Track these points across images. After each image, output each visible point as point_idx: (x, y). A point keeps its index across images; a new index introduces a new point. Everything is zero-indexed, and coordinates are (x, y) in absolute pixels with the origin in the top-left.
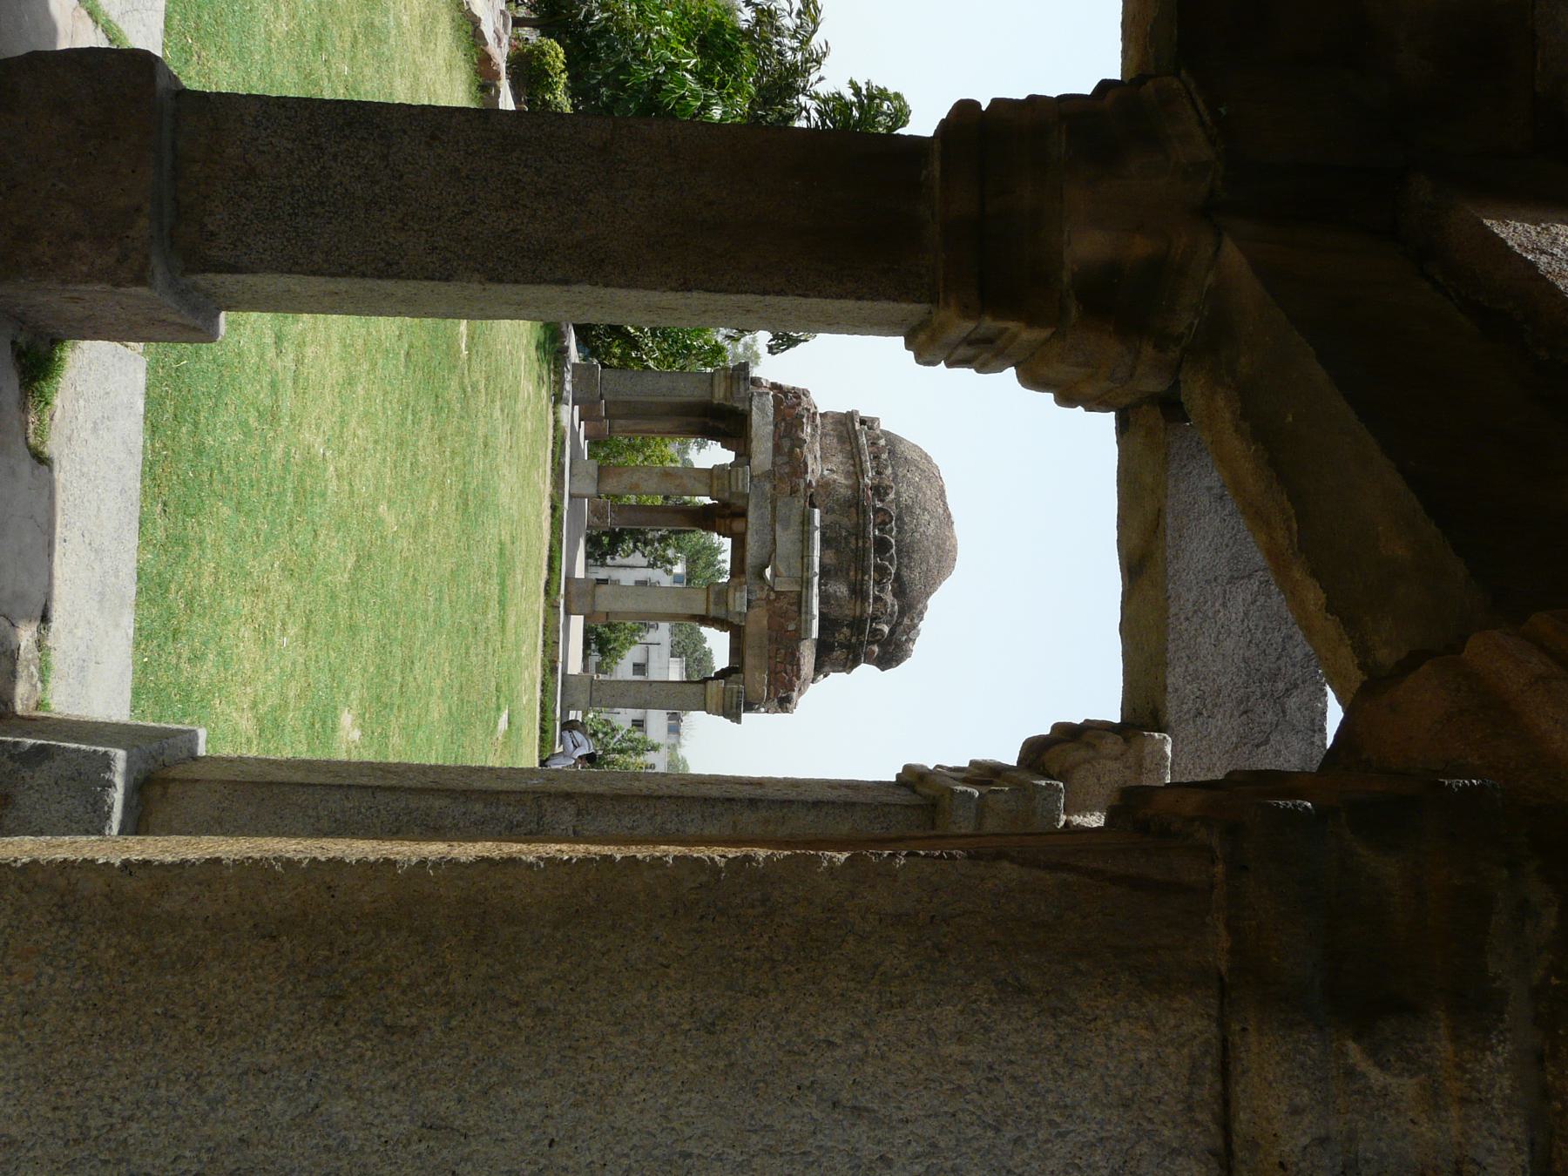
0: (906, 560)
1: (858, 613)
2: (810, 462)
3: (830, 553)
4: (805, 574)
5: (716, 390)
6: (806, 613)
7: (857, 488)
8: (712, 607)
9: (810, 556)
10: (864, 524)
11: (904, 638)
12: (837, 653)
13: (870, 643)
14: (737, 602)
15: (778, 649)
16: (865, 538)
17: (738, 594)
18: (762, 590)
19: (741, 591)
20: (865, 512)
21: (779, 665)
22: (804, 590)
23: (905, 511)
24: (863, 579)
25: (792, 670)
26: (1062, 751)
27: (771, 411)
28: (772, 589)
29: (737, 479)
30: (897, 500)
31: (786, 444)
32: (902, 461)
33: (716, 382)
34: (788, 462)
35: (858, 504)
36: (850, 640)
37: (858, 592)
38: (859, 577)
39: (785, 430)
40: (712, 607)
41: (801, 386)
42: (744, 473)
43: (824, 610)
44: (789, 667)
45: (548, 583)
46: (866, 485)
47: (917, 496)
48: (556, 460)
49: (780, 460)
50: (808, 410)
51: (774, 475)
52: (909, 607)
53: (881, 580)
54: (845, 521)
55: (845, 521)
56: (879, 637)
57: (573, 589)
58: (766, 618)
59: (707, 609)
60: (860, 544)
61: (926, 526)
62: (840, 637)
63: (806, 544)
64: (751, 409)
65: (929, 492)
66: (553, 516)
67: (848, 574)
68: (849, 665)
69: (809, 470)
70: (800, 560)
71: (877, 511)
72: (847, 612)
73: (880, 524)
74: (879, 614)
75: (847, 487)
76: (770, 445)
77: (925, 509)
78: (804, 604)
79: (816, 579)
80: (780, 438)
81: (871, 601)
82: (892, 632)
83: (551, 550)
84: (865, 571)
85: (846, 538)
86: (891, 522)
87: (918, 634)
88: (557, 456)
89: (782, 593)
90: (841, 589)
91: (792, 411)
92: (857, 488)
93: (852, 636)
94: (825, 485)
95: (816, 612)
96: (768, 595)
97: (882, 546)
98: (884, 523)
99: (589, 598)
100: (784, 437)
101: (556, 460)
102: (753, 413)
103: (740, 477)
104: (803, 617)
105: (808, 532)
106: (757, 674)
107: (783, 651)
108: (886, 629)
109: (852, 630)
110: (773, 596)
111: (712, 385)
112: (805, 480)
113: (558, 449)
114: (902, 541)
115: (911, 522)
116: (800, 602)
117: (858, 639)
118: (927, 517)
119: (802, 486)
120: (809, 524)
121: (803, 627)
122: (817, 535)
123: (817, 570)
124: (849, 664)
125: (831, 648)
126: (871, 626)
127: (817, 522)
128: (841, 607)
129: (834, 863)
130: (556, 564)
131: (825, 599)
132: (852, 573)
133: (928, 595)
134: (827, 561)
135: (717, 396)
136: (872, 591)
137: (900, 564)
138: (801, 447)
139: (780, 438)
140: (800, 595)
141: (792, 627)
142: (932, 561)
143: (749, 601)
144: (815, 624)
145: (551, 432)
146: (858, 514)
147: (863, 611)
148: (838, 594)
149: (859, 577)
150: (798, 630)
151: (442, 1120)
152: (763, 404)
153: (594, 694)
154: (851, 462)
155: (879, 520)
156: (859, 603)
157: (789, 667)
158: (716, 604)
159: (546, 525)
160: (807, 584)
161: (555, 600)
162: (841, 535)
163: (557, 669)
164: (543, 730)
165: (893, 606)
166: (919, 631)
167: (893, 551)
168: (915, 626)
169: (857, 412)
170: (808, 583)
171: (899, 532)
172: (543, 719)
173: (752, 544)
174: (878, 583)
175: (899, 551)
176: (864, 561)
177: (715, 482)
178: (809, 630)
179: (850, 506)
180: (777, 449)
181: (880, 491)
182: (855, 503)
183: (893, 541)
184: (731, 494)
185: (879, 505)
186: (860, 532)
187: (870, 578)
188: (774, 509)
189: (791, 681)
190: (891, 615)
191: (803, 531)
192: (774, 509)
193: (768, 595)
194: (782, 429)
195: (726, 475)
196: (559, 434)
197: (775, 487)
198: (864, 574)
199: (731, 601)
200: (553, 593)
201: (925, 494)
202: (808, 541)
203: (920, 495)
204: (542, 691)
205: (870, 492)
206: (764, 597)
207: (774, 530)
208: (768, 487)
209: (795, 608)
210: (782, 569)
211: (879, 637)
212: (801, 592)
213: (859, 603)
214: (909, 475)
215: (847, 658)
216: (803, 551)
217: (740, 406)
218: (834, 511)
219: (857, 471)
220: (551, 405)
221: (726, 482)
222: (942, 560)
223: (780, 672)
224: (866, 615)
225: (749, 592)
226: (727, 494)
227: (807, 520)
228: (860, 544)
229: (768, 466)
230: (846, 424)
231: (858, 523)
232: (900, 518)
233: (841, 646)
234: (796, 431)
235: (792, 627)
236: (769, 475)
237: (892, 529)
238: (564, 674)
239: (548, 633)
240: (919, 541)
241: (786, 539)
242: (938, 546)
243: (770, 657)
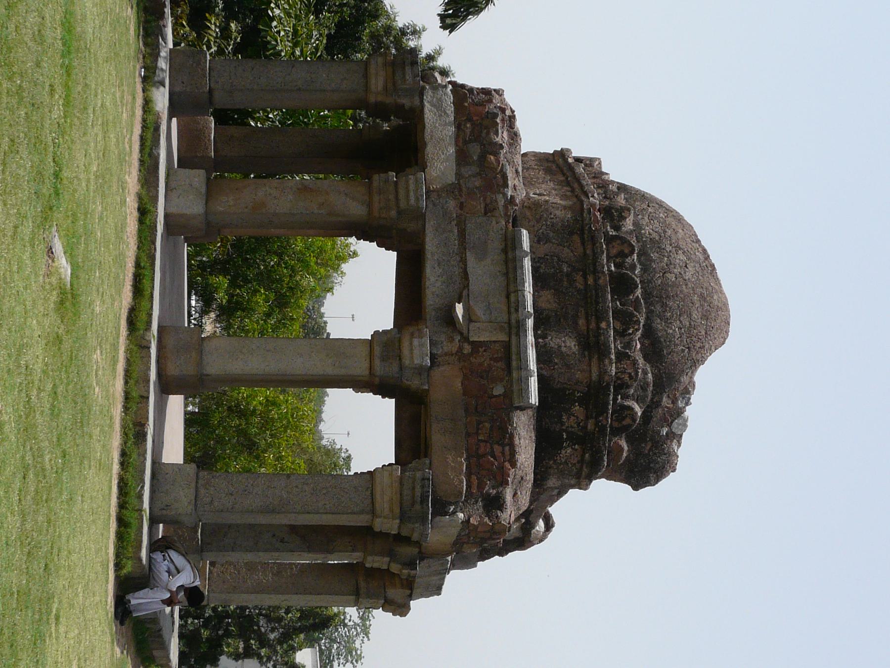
1: (595, 376)
2: (510, 174)
3: (547, 295)
4: (514, 316)
5: (373, 81)
6: (520, 368)
8: (377, 362)
9: (519, 291)
10: (594, 254)
11: (664, 431)
13: (616, 432)
14: (416, 352)
15: (479, 423)
16: (596, 272)
17: (416, 342)
18: (451, 340)
19: (421, 337)
20: (593, 239)
21: (482, 445)
22: (514, 338)
24: (599, 328)
25: (503, 453)
27: (451, 110)
28: (465, 339)
29: (408, 191)
31: (475, 150)
33: (372, 70)
34: (479, 174)
35: (582, 230)
36: (585, 427)
38: (593, 325)
39: (472, 132)
40: (377, 362)
41: (493, 86)
42: (417, 181)
43: (544, 372)
44: (497, 449)
45: (132, 311)
46: (593, 205)
47: (665, 232)
48: (147, 150)
49: (467, 171)
50: (503, 110)
51: (460, 190)
53: (625, 330)
54: (566, 253)
55: (566, 253)
56: (627, 421)
57: (170, 342)
58: (459, 380)
59: (371, 368)
60: (591, 281)
62: (569, 422)
63: (511, 276)
64: (422, 106)
66: (141, 221)
67: (576, 323)
70: (504, 299)
71: (610, 240)
72: (578, 375)
73: (616, 256)
74: (627, 378)
75: (565, 208)
76: (452, 150)
77: (678, 248)
78: (514, 357)
79: (530, 323)
80: (466, 142)
81: (613, 357)
82: (647, 416)
83: (138, 265)
84: (600, 317)
85: (568, 275)
86: (632, 252)
87: (685, 426)
88: (148, 143)
90: (569, 344)
91: (480, 108)
93: (587, 418)
94: (533, 207)
98: (622, 255)
99: (194, 354)
100: (470, 141)
101: (147, 150)
102: (426, 110)
103: (412, 187)
105: (514, 259)
106: (450, 459)
107: (487, 425)
108: (639, 410)
109: (587, 409)
110: (467, 349)
111: (366, 76)
112: (505, 195)
113: (149, 135)
114: (650, 282)
117: (596, 424)
119: (501, 202)
121: (515, 387)
122: (527, 263)
123: (530, 309)
124: (585, 470)
125: (558, 445)
126: (615, 399)
127: (526, 244)
128: (568, 366)
130: (146, 282)
132: (582, 322)
133: (695, 364)
134: (543, 305)
135: (373, 87)
136: (614, 345)
137: (650, 312)
138: (496, 154)
139: (466, 142)
140: (507, 346)
141: (498, 390)
142: (695, 315)
145: (139, 112)
146: (583, 244)
147: (603, 372)
148: (564, 349)
149: (593, 325)
150: (508, 395)
152: (440, 100)
153: (202, 491)
155: (614, 251)
156: (595, 361)
157: (497, 449)
158: (383, 359)
159: (132, 226)
160: (520, 327)
161: (143, 338)
162: (561, 271)
163: (145, 435)
164: (121, 522)
165: (645, 373)
166: (686, 420)
167: (639, 292)
168: (678, 413)
169: (568, 150)
170: (518, 327)
171: (645, 269)
172: (122, 506)
173: (432, 279)
174: (620, 334)
175: (647, 295)
176: (597, 303)
177: (376, 198)
178: (524, 391)
179: (571, 233)
180: (462, 157)
184: (400, 213)
185: (612, 233)
186: (589, 265)
187: (608, 325)
188: (462, 234)
189: (501, 468)
190: (644, 388)
191: (506, 262)
192: (462, 234)
193: (461, 349)
194: (468, 131)
195: (392, 188)
196: (150, 118)
197: (461, 206)
198: (599, 320)
199: (406, 352)
200: (141, 325)
202: (515, 269)
204: (122, 464)
205: (598, 214)
206: (454, 350)
207: (464, 261)
208: (452, 204)
210: (479, 311)
211: (627, 421)
213: (595, 361)
215: (582, 461)
216: (508, 285)
217: (406, 102)
218: (548, 240)
220: (139, 87)
221: (392, 197)
223: (484, 455)
224: (606, 378)
225: (433, 343)
226: (393, 213)
227: (511, 244)
228: (591, 281)
229: (451, 178)
231: (585, 254)
232: (643, 253)
234: (488, 133)
236: (453, 190)
238: (156, 462)
239: (132, 382)
240: (675, 285)
242: (702, 296)
243: (468, 435)
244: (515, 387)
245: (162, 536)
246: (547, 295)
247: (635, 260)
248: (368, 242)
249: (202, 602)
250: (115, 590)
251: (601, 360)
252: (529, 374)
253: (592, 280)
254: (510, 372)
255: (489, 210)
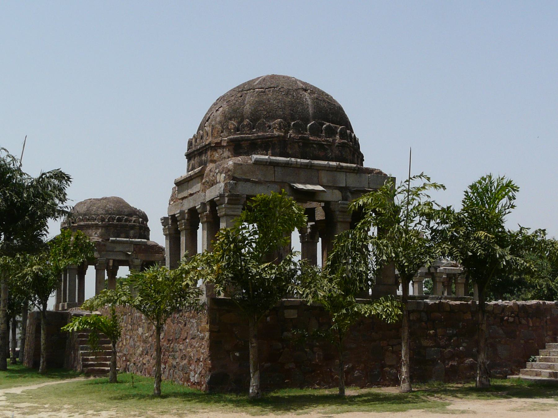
0: (123, 213)
3: (121, 235)
7: (102, 227)
9: (124, 241)
12: (146, 233)
16: (117, 225)
20: (110, 224)
23: (107, 212)
26: (535, 358)
30: (105, 214)
32: (88, 212)
37: (133, 227)
46: (102, 224)
47: (102, 208)
52: (134, 212)
60: (119, 226)
61: (110, 206)
65: (99, 204)
67: (127, 230)
68: (148, 230)
69: (98, 240)
75: (102, 229)
79: (130, 240)
81: (135, 224)
84: (127, 225)
89: (134, 250)
90: (132, 232)
92: (102, 227)
94: (101, 236)
95: (139, 240)
96: (134, 253)
97: (119, 220)
104: (141, 243)
110: (135, 252)
115: (111, 211)
116: (136, 244)
118: (108, 206)
119: (102, 243)
120: (115, 241)
122: (118, 239)
123: (128, 239)
129: (40, 252)
131: (135, 237)
132: (127, 229)
136: (132, 223)
141: (143, 247)
142: (122, 205)
143: (136, 259)
144: (143, 240)
151: (303, 102)
154: (91, 228)
157: (154, 248)
160: (132, 242)
171: (114, 215)
181: (103, 220)
182: (106, 227)
183: (117, 217)
185: (107, 220)
193: (134, 253)
197: (103, 251)
198: (128, 226)
201: (100, 206)
203: (101, 207)
207: (116, 251)
209: (138, 246)
212: (134, 244)
213: (136, 228)
214: (94, 210)
219: (97, 226)
222: (119, 202)
230: (74, 228)
232: (110, 214)
233: (144, 233)
235: (143, 247)
237: (114, 217)
241: (119, 248)
244: (144, 244)
245: (289, 234)
246: (121, 235)
247: (124, 219)
248: (85, 276)
249: (209, 326)
250: (323, 164)
251: (135, 226)
252: (141, 241)
253: (453, 286)
254: (140, 244)
255: (104, 245)
